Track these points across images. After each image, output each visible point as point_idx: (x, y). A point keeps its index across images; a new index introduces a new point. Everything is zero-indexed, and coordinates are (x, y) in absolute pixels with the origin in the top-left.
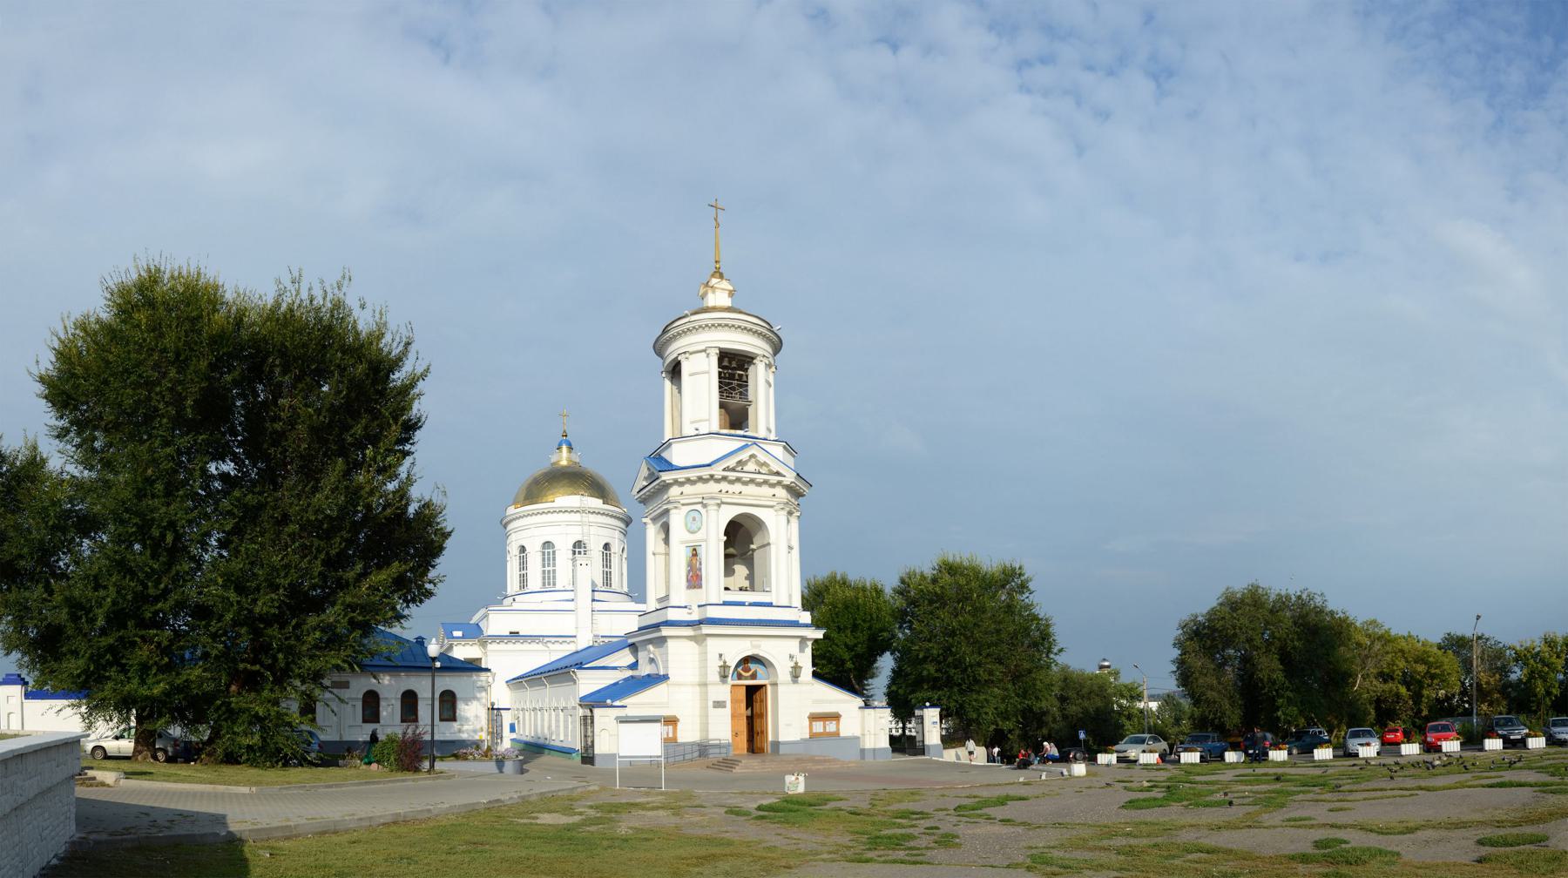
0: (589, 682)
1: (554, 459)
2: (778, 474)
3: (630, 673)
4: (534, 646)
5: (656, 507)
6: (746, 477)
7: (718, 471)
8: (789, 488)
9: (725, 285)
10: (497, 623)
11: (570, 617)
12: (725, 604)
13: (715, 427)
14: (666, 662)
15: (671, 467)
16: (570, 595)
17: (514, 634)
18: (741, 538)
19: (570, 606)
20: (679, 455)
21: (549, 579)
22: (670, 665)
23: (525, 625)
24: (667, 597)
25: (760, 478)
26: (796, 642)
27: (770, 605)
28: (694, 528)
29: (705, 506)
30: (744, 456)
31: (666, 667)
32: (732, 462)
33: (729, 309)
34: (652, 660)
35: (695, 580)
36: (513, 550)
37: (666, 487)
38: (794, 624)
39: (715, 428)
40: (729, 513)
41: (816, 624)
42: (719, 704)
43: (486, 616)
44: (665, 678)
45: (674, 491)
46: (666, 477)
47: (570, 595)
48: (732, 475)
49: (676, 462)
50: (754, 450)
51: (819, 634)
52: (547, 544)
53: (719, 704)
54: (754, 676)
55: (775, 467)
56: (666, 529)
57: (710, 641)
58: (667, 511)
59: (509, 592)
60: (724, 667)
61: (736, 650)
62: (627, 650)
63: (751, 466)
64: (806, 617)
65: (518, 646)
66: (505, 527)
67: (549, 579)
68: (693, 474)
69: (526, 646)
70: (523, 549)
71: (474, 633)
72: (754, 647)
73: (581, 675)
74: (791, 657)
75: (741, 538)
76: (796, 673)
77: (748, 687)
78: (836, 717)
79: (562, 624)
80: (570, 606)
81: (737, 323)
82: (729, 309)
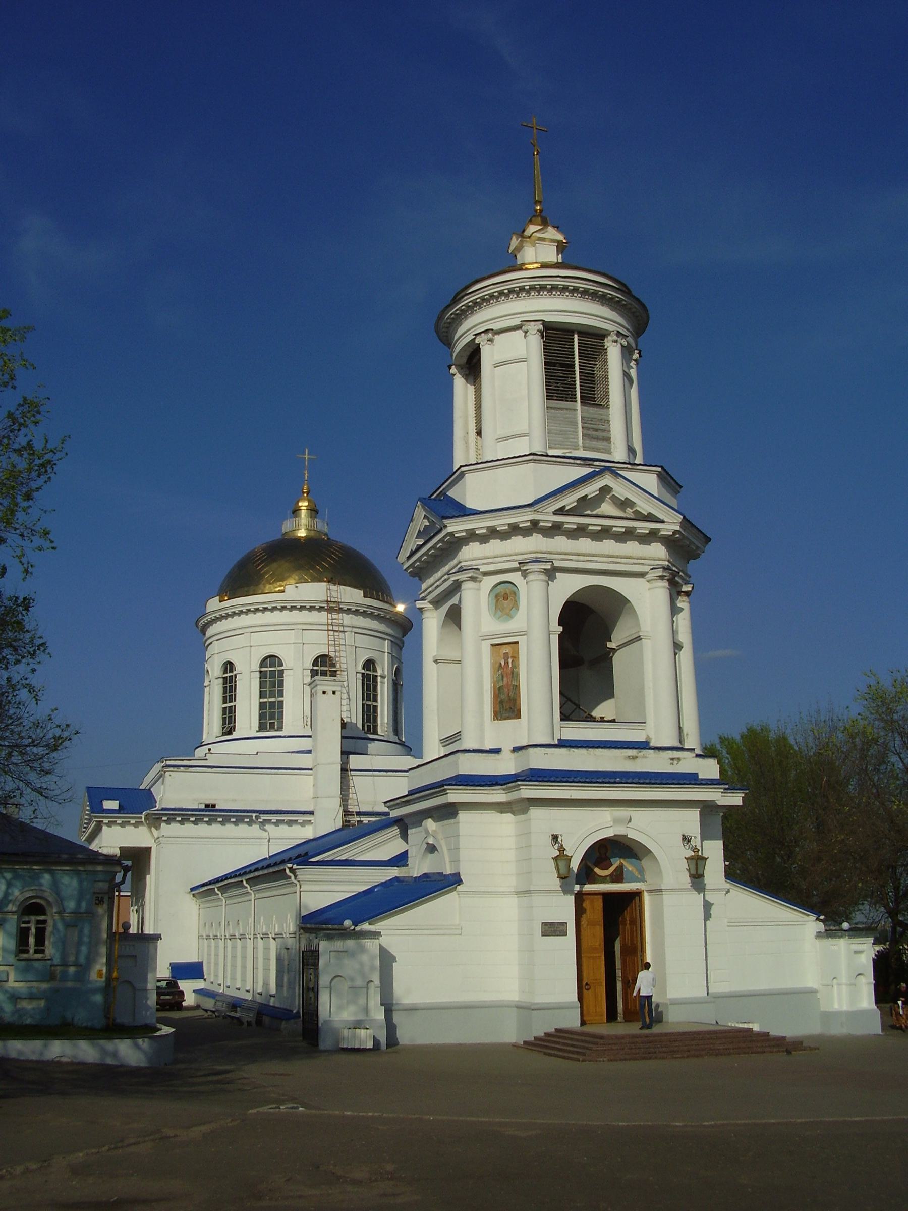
0: (322, 889)
1: (287, 526)
2: (650, 518)
3: (394, 872)
4: (243, 830)
5: (436, 582)
6: (595, 523)
7: (547, 517)
8: (670, 542)
9: (552, 233)
10: (175, 789)
11: (307, 780)
12: (563, 744)
14: (455, 850)
15: (463, 511)
16: (305, 744)
17: (210, 807)
18: (587, 636)
19: (305, 761)
20: (474, 492)
21: (271, 717)
22: (464, 854)
23: (228, 792)
24: (456, 737)
25: (620, 526)
26: (694, 815)
27: (644, 746)
29: (525, 574)
30: (591, 490)
31: (456, 861)
32: (569, 500)
33: (557, 266)
34: (432, 849)
35: (507, 706)
36: (214, 668)
37: (454, 544)
38: (691, 780)
39: (538, 448)
40: (568, 586)
41: (725, 781)
42: (553, 929)
43: (160, 776)
44: (455, 880)
45: (470, 553)
46: (456, 527)
47: (305, 744)
48: (571, 522)
49: (471, 503)
50: (607, 480)
51: (736, 799)
52: (271, 660)
53: (553, 929)
54: (618, 877)
55: (645, 506)
56: (454, 617)
57: (536, 813)
58: (456, 587)
59: (206, 738)
60: (562, 857)
61: (600, 824)
62: (395, 831)
63: (606, 508)
64: (710, 769)
65: (216, 829)
66: (203, 631)
67: (271, 717)
68: (501, 522)
69: (230, 829)
70: (229, 666)
71: (137, 803)
72: (617, 821)
73: (305, 873)
74: (686, 839)
75: (587, 636)
76: (697, 864)
77: (608, 897)
79: (296, 792)
80: (305, 761)
81: (571, 284)
82: (557, 266)
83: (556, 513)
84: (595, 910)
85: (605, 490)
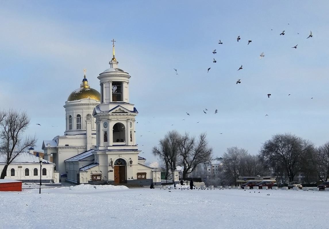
2: (127, 113)
12: (113, 146)
13: (111, 101)
28: (106, 127)
30: (117, 109)
35: (106, 139)
78: (145, 174)
83: (112, 113)
84: (118, 168)
85: (120, 109)
